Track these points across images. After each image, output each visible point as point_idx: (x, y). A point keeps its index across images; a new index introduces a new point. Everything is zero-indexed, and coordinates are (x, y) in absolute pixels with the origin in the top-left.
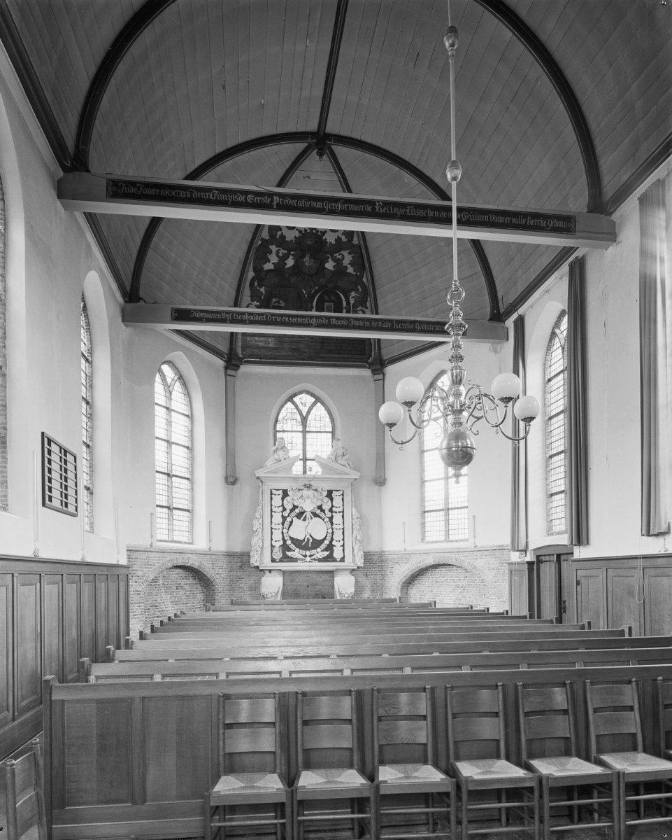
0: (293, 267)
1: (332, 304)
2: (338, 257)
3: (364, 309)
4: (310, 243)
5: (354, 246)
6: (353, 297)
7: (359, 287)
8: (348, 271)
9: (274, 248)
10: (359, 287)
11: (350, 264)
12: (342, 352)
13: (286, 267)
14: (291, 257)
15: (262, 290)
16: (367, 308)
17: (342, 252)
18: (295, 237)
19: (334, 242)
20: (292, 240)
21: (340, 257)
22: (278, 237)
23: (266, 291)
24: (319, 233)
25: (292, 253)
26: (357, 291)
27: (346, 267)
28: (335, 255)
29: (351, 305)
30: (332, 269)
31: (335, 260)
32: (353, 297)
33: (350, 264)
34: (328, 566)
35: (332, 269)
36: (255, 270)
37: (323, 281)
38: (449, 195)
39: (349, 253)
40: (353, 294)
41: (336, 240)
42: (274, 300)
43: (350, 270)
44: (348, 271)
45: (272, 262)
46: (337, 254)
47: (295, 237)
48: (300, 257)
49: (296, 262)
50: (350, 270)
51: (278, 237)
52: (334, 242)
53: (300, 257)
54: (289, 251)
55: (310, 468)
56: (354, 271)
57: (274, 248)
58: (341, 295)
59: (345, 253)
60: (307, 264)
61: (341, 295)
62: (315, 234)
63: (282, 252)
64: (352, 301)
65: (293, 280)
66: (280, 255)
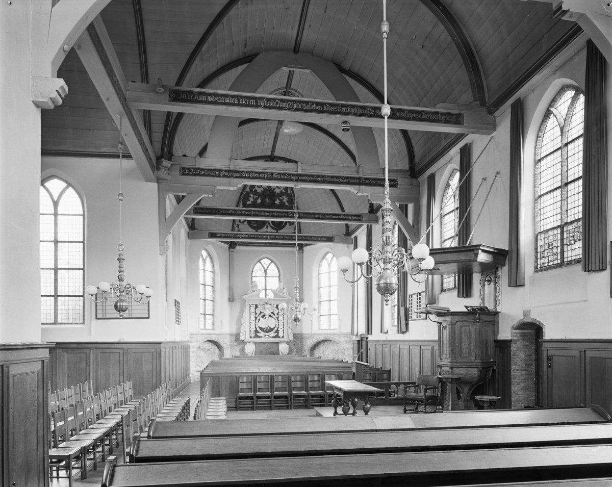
5: (288, 194)
9: (252, 195)
31: (279, 199)
57: (252, 195)
59: (284, 197)
63: (255, 197)
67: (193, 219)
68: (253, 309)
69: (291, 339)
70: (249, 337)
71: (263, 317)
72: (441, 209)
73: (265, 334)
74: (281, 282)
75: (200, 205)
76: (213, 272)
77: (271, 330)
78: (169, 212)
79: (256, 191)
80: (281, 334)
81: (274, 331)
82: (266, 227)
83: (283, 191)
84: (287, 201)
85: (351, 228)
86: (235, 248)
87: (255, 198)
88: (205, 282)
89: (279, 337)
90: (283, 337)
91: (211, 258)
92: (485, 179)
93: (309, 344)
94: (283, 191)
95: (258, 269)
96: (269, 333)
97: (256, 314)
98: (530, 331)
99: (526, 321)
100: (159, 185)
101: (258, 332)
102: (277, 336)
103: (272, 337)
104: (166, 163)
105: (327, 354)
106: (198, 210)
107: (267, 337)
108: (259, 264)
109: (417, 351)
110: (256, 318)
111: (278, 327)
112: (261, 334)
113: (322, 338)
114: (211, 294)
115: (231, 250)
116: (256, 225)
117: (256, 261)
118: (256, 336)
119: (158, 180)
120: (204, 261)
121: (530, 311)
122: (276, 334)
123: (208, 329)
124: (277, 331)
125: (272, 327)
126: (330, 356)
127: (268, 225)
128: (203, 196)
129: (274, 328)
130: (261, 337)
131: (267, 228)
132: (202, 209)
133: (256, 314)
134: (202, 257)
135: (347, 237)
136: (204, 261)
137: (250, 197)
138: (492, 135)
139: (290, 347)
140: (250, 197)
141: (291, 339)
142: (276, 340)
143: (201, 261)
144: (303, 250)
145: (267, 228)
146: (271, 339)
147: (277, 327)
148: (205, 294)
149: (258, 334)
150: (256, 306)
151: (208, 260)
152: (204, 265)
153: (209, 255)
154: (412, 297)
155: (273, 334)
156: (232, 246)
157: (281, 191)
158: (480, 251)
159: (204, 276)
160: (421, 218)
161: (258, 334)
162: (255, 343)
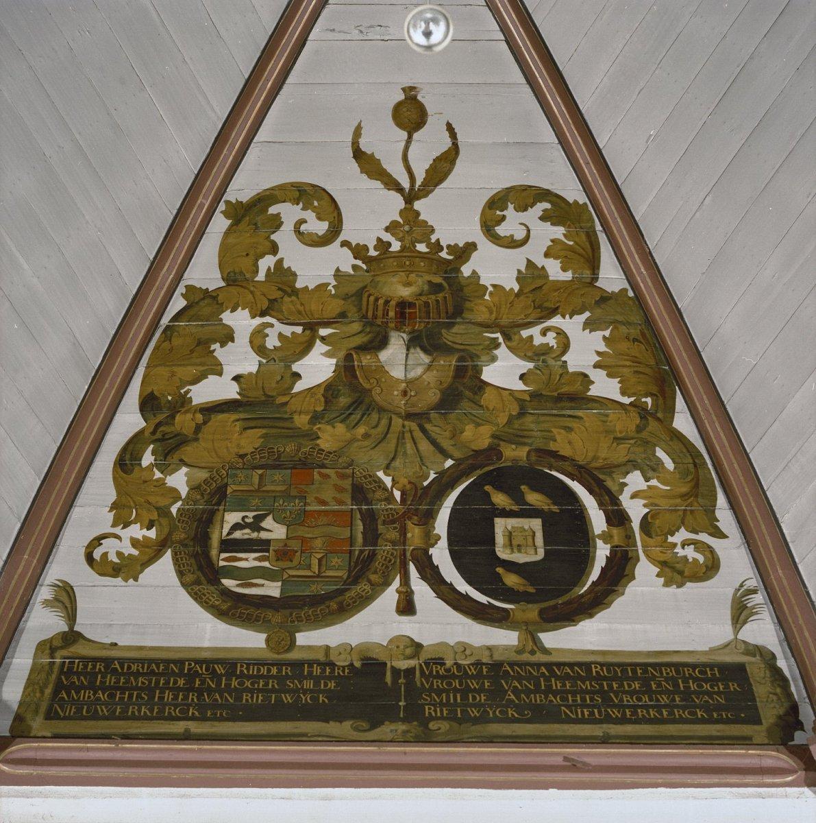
0: (329, 390)
1: (536, 524)
2: (538, 340)
3: (704, 537)
4: (405, 292)
5: (605, 298)
6: (634, 496)
7: (660, 453)
8: (594, 391)
9: (241, 321)
10: (660, 453)
11: (597, 366)
12: (615, 713)
13: (299, 387)
14: (319, 347)
15: (179, 480)
16: (720, 535)
17: (556, 321)
18: (338, 274)
19: (512, 285)
20: (322, 287)
21: (551, 339)
22: (261, 277)
23: (194, 488)
24: (444, 254)
25: (324, 332)
26: (651, 468)
27: (585, 379)
28: (525, 333)
29: (636, 525)
30: (520, 386)
31: (524, 350)
32: (634, 496)
33: (597, 366)
34: (88, 749)
35: (520, 386)
36: (148, 404)
37: (478, 436)
38: (813, 788)
39: (590, 325)
40: (635, 480)
41: (520, 278)
42: (232, 518)
43: (605, 387)
44: (594, 391)
45: (231, 370)
46: (535, 331)
47: (338, 274)
48: (362, 348)
49: (347, 369)
50: (605, 387)
51: (261, 277)
52: (512, 285)
53: (362, 348)
54: (311, 327)
55: (513, 732)
56: (623, 393)
57: (241, 321)
58: (576, 487)
59: (572, 325)
60: (397, 373)
61: (576, 487)
62: (422, 256)
63: (277, 332)
64: (636, 510)
65: (330, 437)
66: (272, 342)
72: (360, 397)
74: (145, 502)
79: (283, 277)
82: (390, 596)
83: (555, 271)
87: (272, 342)
94: (555, 271)
98: (582, 591)
116: (273, 589)
121: (663, 586)
127: (421, 589)
131: (407, 607)
137: (228, 337)
140: (228, 337)
145: (407, 607)
157: (532, 276)
160: (207, 403)
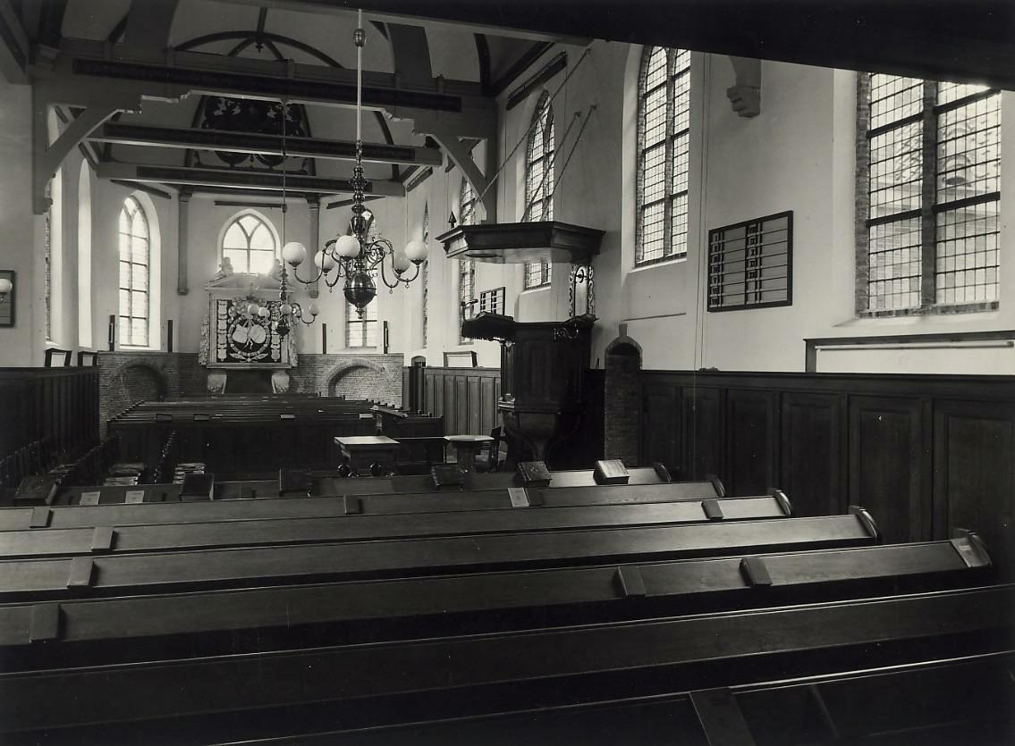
31: (275, 110)
67: (108, 145)
68: (223, 310)
69: (293, 365)
70: (215, 360)
71: (242, 323)
73: (245, 354)
75: (120, 120)
76: (148, 240)
77: (257, 346)
78: (54, 133)
80: (275, 356)
81: (262, 349)
84: (290, 113)
85: (401, 171)
86: (191, 195)
88: (131, 255)
89: (273, 361)
90: (279, 361)
91: (144, 213)
92: (578, 114)
93: (326, 373)
95: (233, 237)
96: (253, 354)
97: (229, 317)
99: (621, 341)
100: (33, 89)
101: (234, 352)
102: (268, 359)
103: (259, 361)
104: (48, 52)
105: (359, 390)
106: (114, 129)
107: (249, 360)
108: (235, 224)
109: (441, 382)
110: (229, 325)
111: (271, 343)
112: (238, 355)
113: (350, 363)
114: (143, 279)
115: (183, 198)
117: (232, 219)
118: (229, 359)
119: (33, 81)
120: (130, 218)
122: (266, 355)
123: (355, 348)
124: (269, 350)
125: (260, 341)
126: (364, 395)
128: (117, 111)
129: (264, 343)
130: (238, 360)
132: (121, 127)
133: (229, 317)
134: (127, 212)
135: (396, 184)
136: (130, 218)
138: (588, 47)
139: (291, 379)
141: (294, 363)
142: (264, 366)
143: (123, 217)
144: (319, 204)
146: (257, 363)
147: (268, 342)
148: (131, 280)
149: (232, 355)
150: (230, 304)
151: (138, 215)
152: (130, 226)
153: (140, 207)
154: (484, 297)
155: (259, 355)
156: (185, 192)
158: (554, 232)
159: (130, 247)
161: (232, 355)
162: (228, 372)
